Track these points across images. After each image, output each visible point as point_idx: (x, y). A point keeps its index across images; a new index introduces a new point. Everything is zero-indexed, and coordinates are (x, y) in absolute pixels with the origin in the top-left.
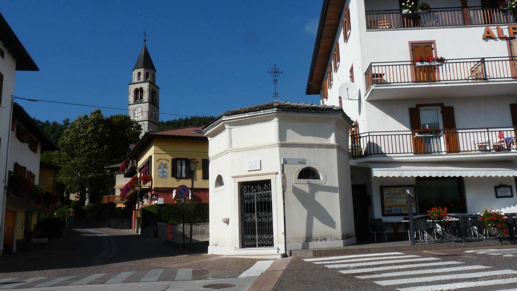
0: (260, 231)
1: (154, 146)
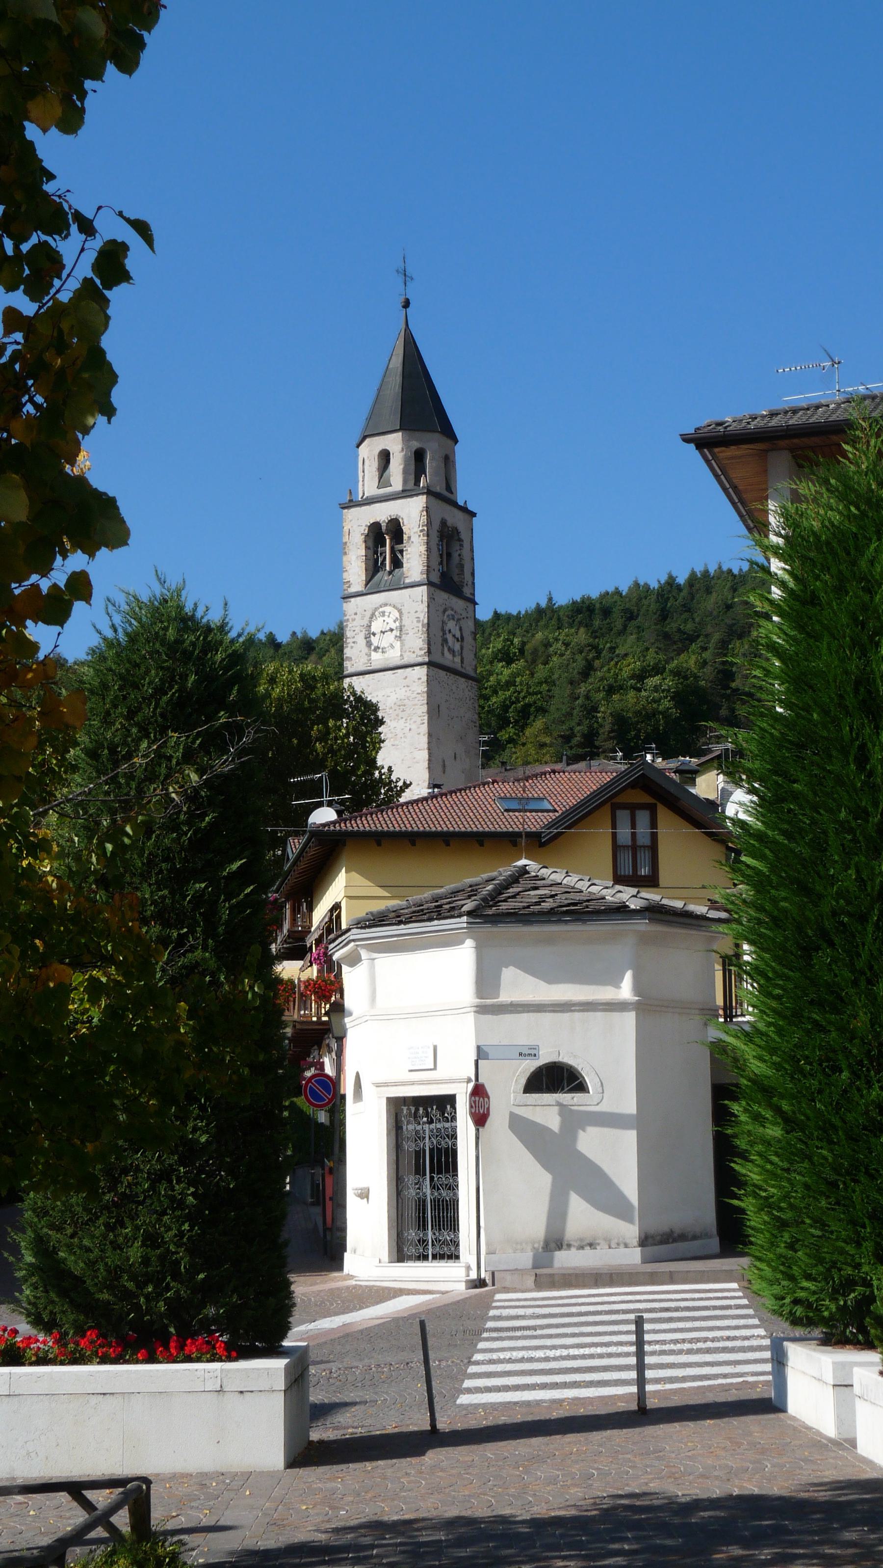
1: (344, 870)
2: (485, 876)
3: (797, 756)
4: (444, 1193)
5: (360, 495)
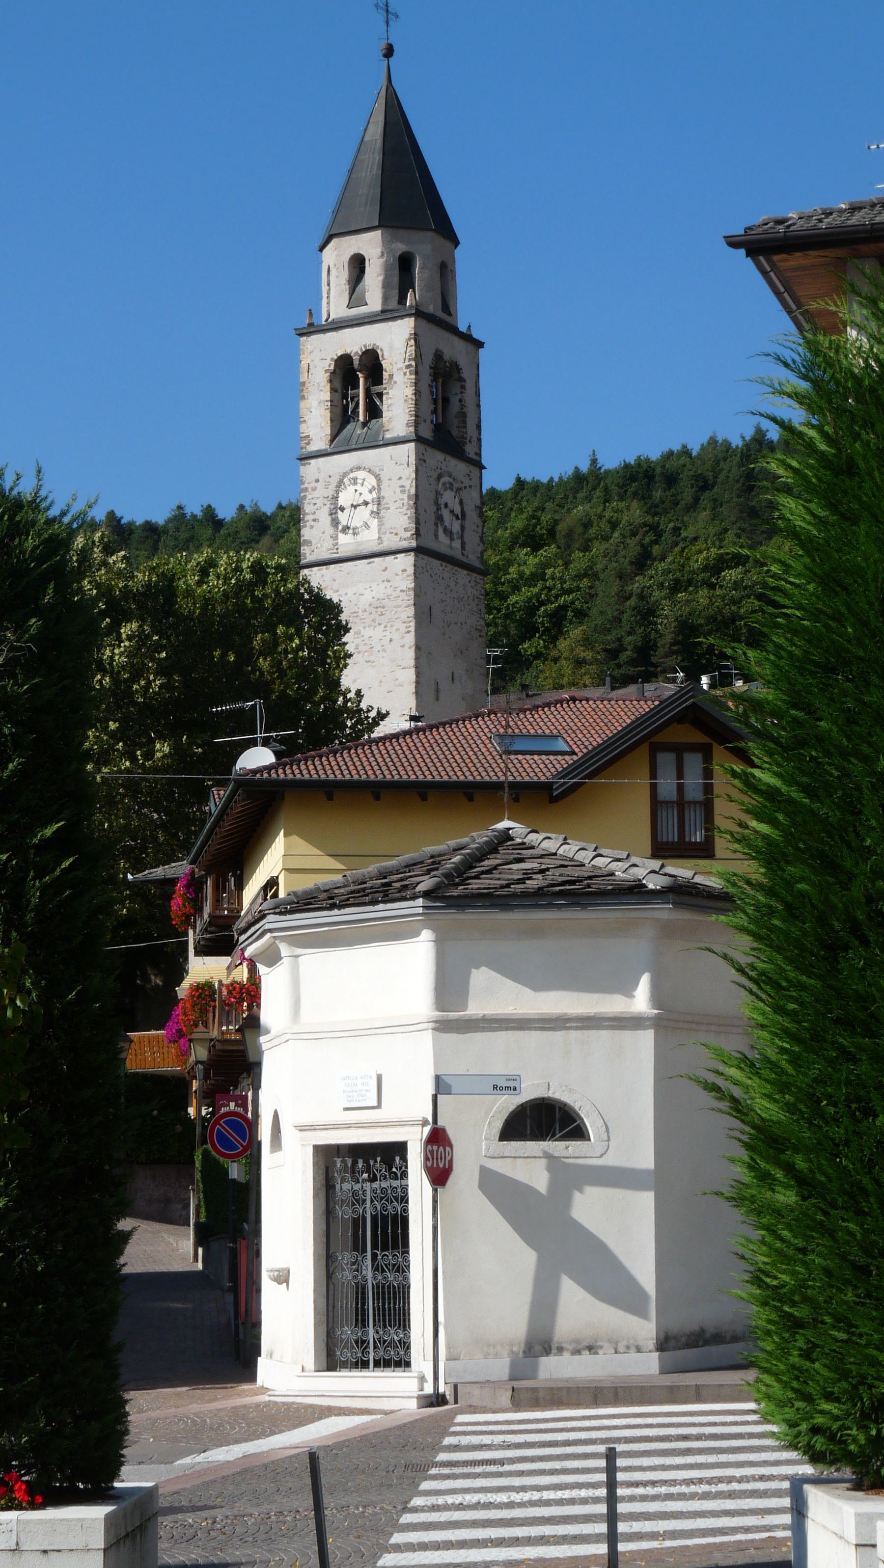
0: (379, 1315)
1: (282, 833)
2: (452, 843)
3: (823, 684)
4: (390, 1276)
5: (324, 317)
